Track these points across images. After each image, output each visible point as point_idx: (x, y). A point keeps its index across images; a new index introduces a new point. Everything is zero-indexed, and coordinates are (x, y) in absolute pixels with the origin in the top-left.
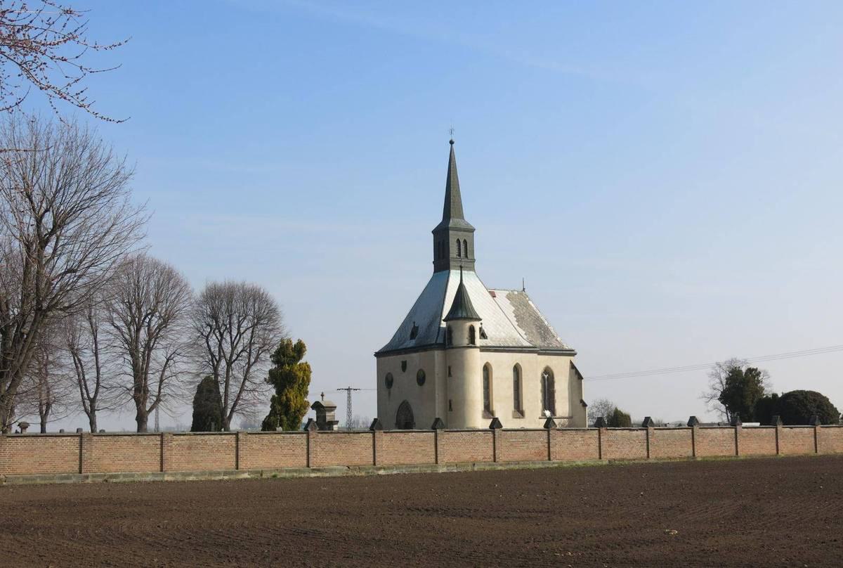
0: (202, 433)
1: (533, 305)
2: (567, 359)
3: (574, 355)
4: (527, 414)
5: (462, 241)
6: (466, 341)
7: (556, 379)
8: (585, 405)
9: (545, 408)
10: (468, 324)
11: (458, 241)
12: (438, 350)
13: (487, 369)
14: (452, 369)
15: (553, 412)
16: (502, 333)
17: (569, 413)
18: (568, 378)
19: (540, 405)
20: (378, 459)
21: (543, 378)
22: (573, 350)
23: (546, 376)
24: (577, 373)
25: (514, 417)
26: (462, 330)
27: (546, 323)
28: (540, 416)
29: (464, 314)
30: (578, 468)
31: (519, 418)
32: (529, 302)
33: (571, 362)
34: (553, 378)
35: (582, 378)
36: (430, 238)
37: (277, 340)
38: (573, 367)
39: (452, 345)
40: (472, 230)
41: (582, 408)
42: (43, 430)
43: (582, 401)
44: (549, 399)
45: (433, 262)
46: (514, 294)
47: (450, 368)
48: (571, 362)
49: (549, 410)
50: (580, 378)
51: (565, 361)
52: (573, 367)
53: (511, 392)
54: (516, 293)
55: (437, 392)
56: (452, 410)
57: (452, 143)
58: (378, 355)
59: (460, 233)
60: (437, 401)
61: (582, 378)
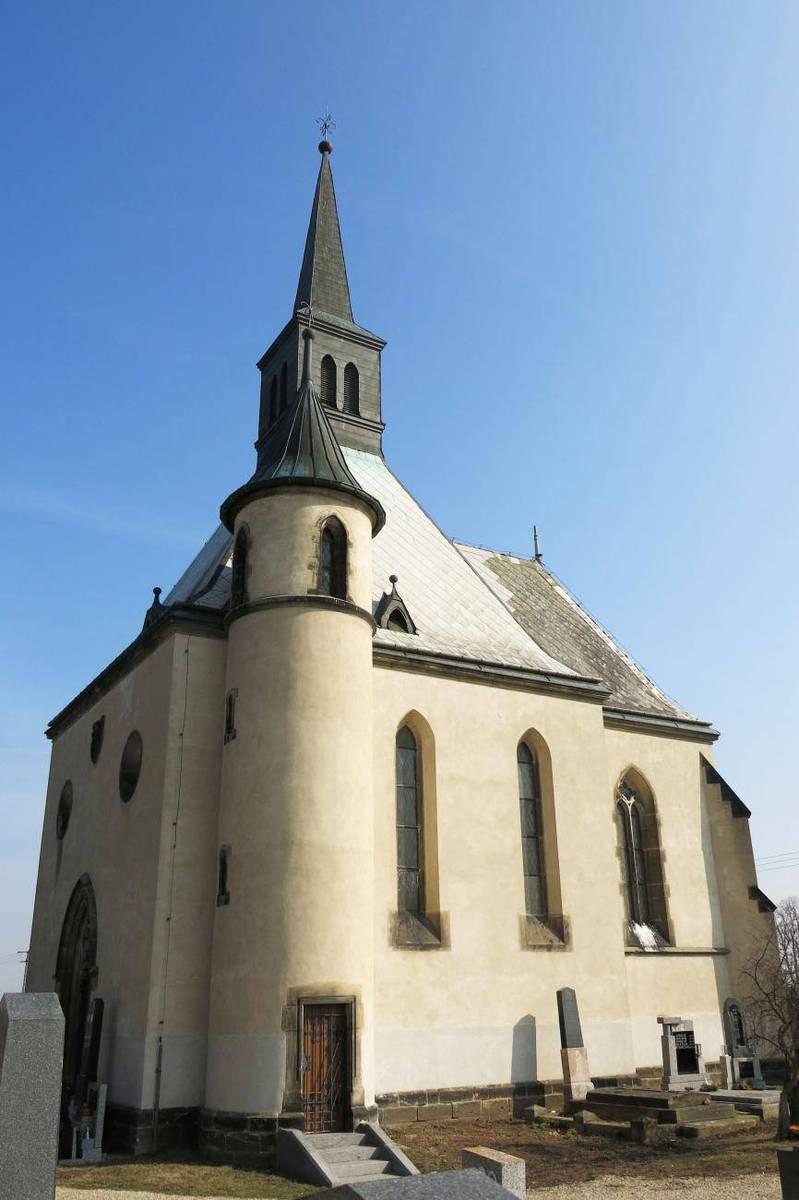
1: (568, 599)
2: (694, 749)
3: (711, 738)
6: (305, 579)
7: (663, 813)
8: (766, 906)
9: (634, 917)
10: (317, 511)
11: (328, 363)
12: (190, 632)
13: (412, 741)
16: (472, 628)
17: (715, 940)
18: (698, 813)
20: (711, 1014)
21: (620, 806)
24: (728, 794)
25: (530, 944)
26: (292, 531)
27: (611, 645)
29: (303, 471)
31: (549, 948)
32: (557, 588)
33: (704, 762)
34: (652, 808)
36: (255, 379)
38: (711, 776)
39: (248, 599)
41: (761, 916)
43: (755, 893)
44: (644, 884)
45: (258, 446)
46: (508, 562)
47: (230, 702)
48: (704, 762)
49: (650, 923)
50: (740, 811)
51: (687, 753)
52: (711, 776)
55: (168, 817)
56: (227, 902)
57: (324, 148)
59: (337, 343)
60: (166, 858)
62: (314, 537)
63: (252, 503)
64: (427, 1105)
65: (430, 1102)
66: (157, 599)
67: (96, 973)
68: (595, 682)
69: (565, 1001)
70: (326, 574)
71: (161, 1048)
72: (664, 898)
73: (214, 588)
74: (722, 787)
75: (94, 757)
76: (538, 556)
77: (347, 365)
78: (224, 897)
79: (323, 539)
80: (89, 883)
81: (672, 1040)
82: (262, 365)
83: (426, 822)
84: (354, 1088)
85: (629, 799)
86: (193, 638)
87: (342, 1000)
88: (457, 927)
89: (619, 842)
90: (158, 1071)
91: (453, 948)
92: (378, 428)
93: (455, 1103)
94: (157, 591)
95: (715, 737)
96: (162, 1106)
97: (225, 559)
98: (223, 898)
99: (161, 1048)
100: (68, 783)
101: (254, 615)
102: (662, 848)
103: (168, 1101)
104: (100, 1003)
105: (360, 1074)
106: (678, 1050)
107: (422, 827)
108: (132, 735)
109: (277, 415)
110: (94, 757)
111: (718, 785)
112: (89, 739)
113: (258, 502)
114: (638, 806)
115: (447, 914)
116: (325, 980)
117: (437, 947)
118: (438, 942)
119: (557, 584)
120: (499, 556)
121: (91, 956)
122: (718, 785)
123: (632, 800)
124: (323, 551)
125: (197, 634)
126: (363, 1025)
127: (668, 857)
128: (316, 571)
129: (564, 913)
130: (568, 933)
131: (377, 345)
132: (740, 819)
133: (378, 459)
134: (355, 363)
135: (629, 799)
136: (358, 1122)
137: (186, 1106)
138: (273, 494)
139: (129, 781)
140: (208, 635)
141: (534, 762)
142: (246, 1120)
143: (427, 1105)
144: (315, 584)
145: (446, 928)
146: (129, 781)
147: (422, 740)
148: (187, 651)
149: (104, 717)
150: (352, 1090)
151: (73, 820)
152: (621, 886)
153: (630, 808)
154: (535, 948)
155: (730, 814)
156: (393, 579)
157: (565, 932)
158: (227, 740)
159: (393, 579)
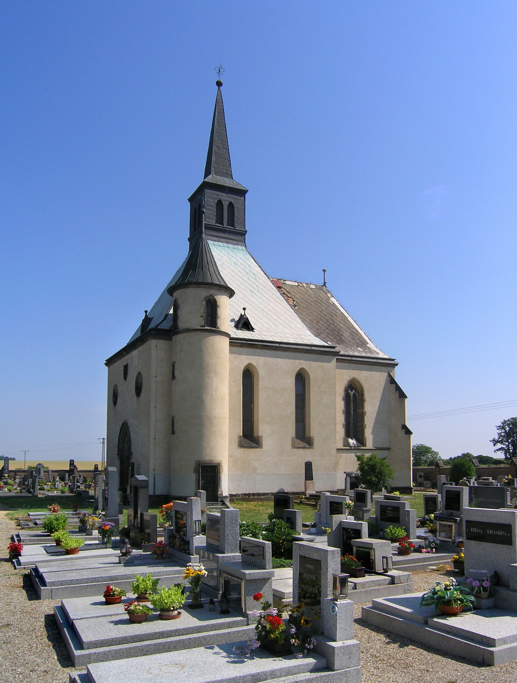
0: (364, 550)
4: (316, 443)
5: (226, 204)
7: (367, 396)
9: (348, 434)
11: (220, 204)
12: (157, 339)
14: (176, 366)
15: (361, 441)
19: (340, 431)
22: (393, 360)
23: (352, 393)
24: (398, 388)
28: (341, 445)
30: (500, 544)
31: (304, 448)
35: (406, 397)
36: (187, 206)
37: (446, 511)
39: (178, 328)
40: (242, 193)
42: (262, 555)
43: (404, 427)
45: (189, 239)
47: (173, 366)
50: (402, 396)
53: (291, 409)
54: (313, 287)
55: (152, 405)
57: (219, 84)
58: (109, 362)
61: (406, 397)
62: (203, 305)
63: (179, 290)
64: (251, 497)
65: (257, 496)
66: (146, 314)
67: (132, 454)
68: (334, 348)
69: (308, 466)
70: (209, 318)
71: (155, 478)
72: (363, 429)
73: (167, 318)
74: (396, 385)
75: (92, 604)
76: (325, 283)
77: (229, 203)
78: (173, 432)
79: (207, 304)
80: (127, 424)
81: (348, 478)
82: (190, 200)
83: (255, 404)
84: (219, 490)
85: (352, 391)
86: (159, 341)
87: (215, 464)
88: (266, 442)
89: (344, 409)
90: (154, 484)
91: (263, 448)
92: (243, 234)
93: (262, 497)
94: (146, 312)
95: (397, 365)
96: (156, 494)
97: (169, 309)
98: (173, 432)
99: (155, 478)
100: (116, 386)
101: (180, 335)
102: (364, 410)
103: (158, 493)
104: (133, 464)
105: (221, 486)
106: (351, 483)
107: (253, 406)
108: (123, 424)
109: (197, 228)
110: (92, 604)
111: (394, 385)
112: (123, 372)
113: (181, 290)
114: (356, 393)
115: (262, 437)
116: (208, 458)
117: (257, 447)
118: (258, 446)
119: (332, 296)
120: (304, 285)
121: (129, 448)
122: (394, 385)
123: (353, 392)
124: (207, 309)
125: (160, 339)
126: (222, 472)
127: (367, 414)
128: (204, 318)
129: (311, 436)
130: (312, 443)
131: (242, 193)
132: (401, 399)
133: (244, 248)
134: (233, 202)
135: (352, 391)
136: (220, 500)
137: (165, 494)
138: (186, 288)
139: (138, 390)
140: (165, 339)
141: (304, 380)
142: (182, 498)
143: (251, 497)
144: (204, 323)
145: (261, 441)
146: (138, 390)
147: (254, 374)
148: (156, 346)
149: (128, 363)
150: (218, 491)
151: (119, 400)
152: (343, 425)
153: (352, 395)
154: (297, 448)
155: (398, 396)
156: (244, 309)
157: (311, 442)
158: (172, 380)
159: (244, 309)
